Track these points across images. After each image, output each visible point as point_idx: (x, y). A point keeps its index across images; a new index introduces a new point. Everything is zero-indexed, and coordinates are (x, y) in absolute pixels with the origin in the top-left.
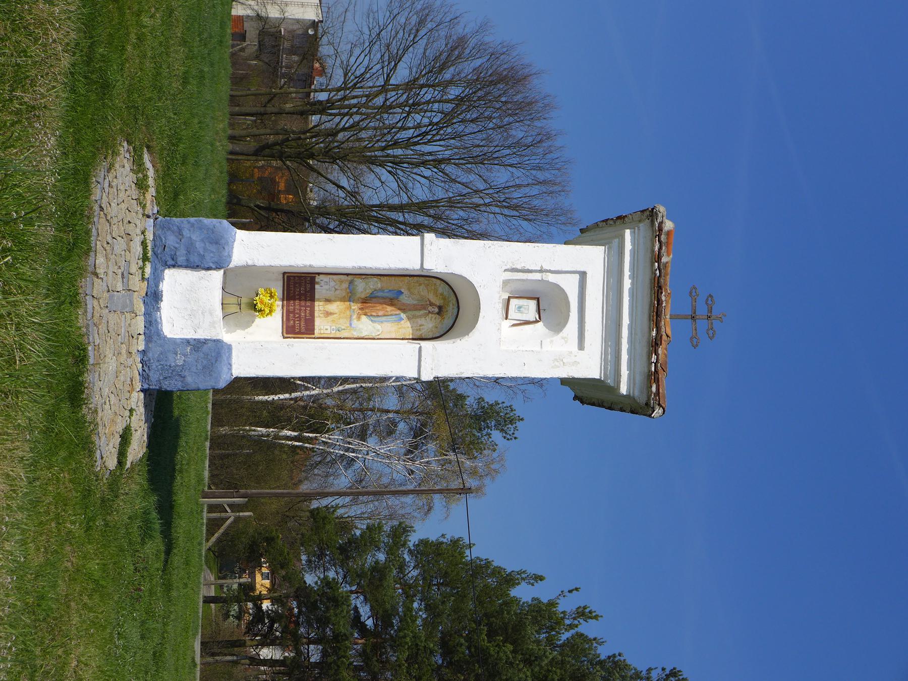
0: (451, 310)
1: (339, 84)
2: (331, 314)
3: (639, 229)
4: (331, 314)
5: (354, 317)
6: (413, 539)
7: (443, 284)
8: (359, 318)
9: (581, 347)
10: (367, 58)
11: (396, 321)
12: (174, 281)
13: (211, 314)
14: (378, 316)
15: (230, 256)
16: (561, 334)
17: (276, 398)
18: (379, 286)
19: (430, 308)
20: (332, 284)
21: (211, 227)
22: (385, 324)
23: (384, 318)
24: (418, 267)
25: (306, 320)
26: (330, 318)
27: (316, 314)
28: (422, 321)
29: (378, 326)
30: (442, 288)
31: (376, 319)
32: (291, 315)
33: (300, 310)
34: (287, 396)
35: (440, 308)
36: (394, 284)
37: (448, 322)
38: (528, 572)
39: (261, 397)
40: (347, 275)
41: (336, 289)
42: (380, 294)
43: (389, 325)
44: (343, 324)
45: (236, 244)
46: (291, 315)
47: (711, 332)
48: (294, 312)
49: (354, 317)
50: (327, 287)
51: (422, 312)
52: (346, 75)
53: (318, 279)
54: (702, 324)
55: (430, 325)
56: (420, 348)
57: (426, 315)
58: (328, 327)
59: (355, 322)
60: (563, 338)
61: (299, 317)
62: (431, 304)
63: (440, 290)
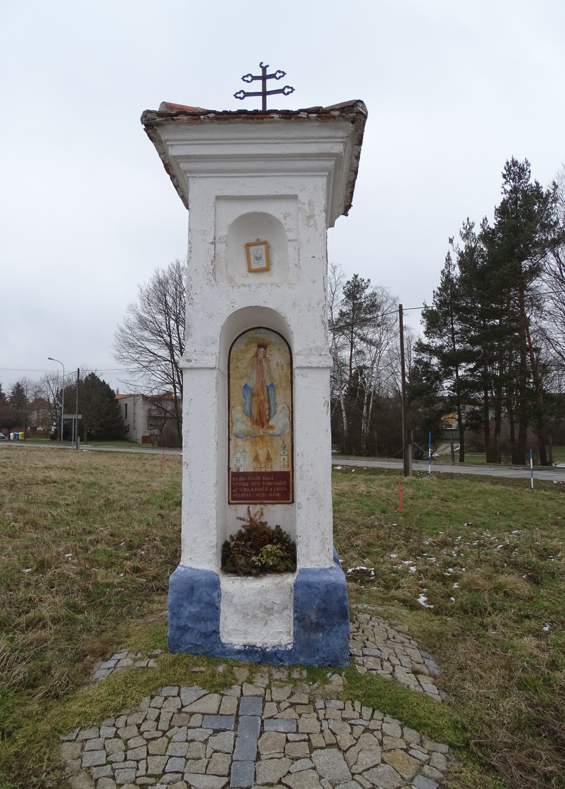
0: (261, 335)
1: (172, 387)
3: (168, 140)
5: (271, 432)
7: (236, 344)
8: (272, 427)
9: (294, 197)
10: (157, 372)
11: (274, 391)
12: (235, 632)
13: (267, 591)
14: (269, 408)
15: (207, 573)
16: (282, 221)
17: (345, 419)
18: (239, 408)
19: (261, 356)
20: (238, 455)
21: (176, 594)
22: (277, 401)
23: (272, 402)
24: (215, 373)
26: (273, 456)
27: (269, 470)
28: (273, 364)
29: (280, 407)
30: (240, 345)
32: (271, 495)
33: (265, 486)
34: (344, 412)
35: (260, 346)
36: (237, 394)
37: (273, 338)
40: (229, 440)
41: (244, 451)
42: (247, 407)
43: (278, 396)
44: (278, 443)
45: (194, 566)
46: (271, 495)
48: (268, 493)
49: (271, 432)
50: (242, 460)
51: (264, 365)
52: (167, 383)
53: (234, 470)
55: (278, 355)
56: (298, 368)
57: (268, 361)
58: (282, 458)
59: (276, 431)
60: (285, 218)
61: (272, 487)
62: (256, 355)
63: (243, 347)
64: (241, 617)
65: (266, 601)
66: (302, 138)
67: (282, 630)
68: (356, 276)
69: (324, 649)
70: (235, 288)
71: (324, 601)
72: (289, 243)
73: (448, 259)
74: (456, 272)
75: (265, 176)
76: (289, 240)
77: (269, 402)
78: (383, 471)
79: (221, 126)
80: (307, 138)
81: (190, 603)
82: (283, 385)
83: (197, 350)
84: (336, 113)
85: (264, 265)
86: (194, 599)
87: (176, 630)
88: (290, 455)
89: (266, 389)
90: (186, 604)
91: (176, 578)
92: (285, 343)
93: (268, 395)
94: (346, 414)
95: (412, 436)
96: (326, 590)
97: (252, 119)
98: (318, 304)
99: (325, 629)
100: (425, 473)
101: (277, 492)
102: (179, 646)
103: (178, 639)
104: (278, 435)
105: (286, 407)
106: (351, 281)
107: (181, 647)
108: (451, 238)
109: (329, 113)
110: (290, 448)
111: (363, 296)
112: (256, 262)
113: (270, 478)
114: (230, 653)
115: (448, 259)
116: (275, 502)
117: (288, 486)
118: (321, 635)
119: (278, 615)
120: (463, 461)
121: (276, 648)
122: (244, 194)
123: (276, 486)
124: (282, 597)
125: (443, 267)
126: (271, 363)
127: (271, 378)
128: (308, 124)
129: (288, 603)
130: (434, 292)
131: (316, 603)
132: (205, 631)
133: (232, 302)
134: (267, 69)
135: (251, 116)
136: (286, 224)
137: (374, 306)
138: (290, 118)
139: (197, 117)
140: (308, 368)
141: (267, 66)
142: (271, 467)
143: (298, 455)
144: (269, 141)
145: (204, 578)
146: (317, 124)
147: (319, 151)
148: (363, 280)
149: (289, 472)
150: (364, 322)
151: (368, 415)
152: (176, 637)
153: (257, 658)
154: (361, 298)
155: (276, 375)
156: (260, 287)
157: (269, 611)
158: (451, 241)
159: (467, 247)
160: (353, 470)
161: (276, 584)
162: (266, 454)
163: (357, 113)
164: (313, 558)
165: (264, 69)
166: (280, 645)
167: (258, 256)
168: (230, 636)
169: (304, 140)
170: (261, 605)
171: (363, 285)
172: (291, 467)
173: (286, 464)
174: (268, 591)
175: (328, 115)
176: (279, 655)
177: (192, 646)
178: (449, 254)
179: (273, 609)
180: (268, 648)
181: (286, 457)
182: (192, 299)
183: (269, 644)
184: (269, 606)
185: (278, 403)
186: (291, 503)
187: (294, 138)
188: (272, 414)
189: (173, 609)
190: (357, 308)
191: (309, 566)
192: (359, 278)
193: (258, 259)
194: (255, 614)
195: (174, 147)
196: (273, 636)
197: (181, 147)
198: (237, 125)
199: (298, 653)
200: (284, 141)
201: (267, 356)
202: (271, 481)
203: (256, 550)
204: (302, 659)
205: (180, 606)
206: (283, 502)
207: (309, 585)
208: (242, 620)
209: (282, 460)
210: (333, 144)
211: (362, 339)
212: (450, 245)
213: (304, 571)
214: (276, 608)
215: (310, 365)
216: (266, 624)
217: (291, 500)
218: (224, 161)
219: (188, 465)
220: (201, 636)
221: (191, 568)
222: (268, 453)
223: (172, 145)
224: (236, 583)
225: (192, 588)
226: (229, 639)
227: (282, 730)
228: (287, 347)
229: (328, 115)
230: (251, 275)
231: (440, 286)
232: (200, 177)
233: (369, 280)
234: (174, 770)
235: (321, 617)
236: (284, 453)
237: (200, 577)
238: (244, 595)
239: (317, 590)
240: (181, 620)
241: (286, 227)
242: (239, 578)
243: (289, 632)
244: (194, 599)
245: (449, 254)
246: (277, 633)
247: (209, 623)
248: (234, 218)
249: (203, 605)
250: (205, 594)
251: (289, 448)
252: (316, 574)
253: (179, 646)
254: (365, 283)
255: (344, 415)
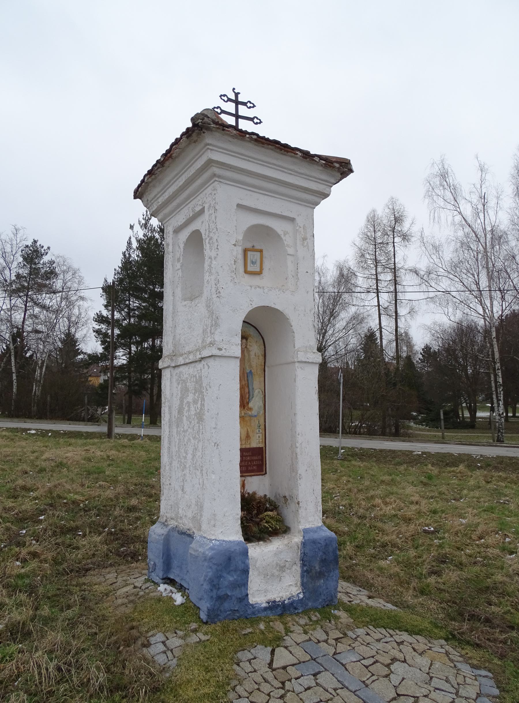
2: (248, 433)
4: (248, 433)
6: (105, 313)
8: (251, 409)
9: (292, 220)
11: (252, 377)
14: (249, 392)
16: (282, 236)
17: (15, 381)
23: (250, 387)
25: (253, 455)
26: (251, 434)
27: (248, 446)
28: (252, 354)
29: (256, 392)
31: (251, 394)
32: (249, 468)
34: (14, 375)
38: (124, 251)
39: (14, 390)
43: (255, 382)
45: (226, 539)
47: (256, 120)
49: (250, 413)
51: (246, 354)
54: (243, 111)
55: (256, 347)
57: (248, 351)
59: (254, 412)
60: (285, 235)
61: (250, 461)
64: (262, 578)
65: (281, 561)
66: (308, 176)
67: (291, 583)
68: (35, 242)
69: (325, 592)
70: (253, 288)
71: (324, 553)
72: (288, 256)
73: (129, 243)
74: (135, 255)
75: (273, 197)
76: (288, 255)
77: (248, 387)
78: (82, 435)
79: (256, 147)
80: (311, 177)
81: (228, 573)
82: (258, 373)
83: (224, 340)
84: (337, 165)
85: (258, 270)
86: (232, 568)
87: (216, 601)
88: (264, 433)
89: (246, 375)
90: (225, 575)
91: (214, 551)
92: (260, 337)
93: (248, 380)
94: (17, 376)
95: (86, 400)
96: (325, 544)
97: (281, 150)
98: (310, 311)
99: (325, 576)
100: (139, 437)
101: (254, 465)
102: (219, 615)
103: (218, 609)
104: (255, 416)
105: (261, 392)
106: (29, 245)
107: (220, 616)
108: (132, 224)
109: (332, 163)
110: (263, 427)
111: (41, 262)
112: (252, 265)
113: (249, 454)
114: (259, 612)
115: (129, 243)
116: (253, 474)
117: (262, 460)
118: (322, 581)
119: (289, 571)
120: (130, 423)
121: (291, 600)
122: (258, 208)
123: (253, 461)
124: (291, 555)
125: (124, 249)
126: (251, 353)
127: (250, 366)
128: (316, 167)
129: (296, 559)
130: (115, 270)
131: (319, 555)
132: (240, 596)
133: (250, 301)
134: (239, 95)
135: (283, 148)
136: (285, 240)
137: (52, 274)
138: (306, 158)
139: (243, 134)
140: (305, 362)
141: (239, 93)
142: (250, 444)
143: (299, 435)
144: (286, 170)
145: (237, 548)
146: (321, 168)
147: (317, 189)
148: (43, 247)
149: (262, 448)
150: (40, 288)
151: (41, 378)
152: (216, 607)
153: (279, 611)
154: (39, 263)
155: (254, 364)
156: (271, 290)
157: (282, 568)
158: (132, 227)
159: (145, 235)
160: (50, 434)
161: (286, 545)
162: (246, 433)
163: (349, 169)
164: (310, 519)
165: (237, 94)
166: (293, 596)
167: (254, 261)
168: (254, 597)
169: (308, 177)
170: (277, 565)
171: (43, 251)
172: (264, 444)
173: (261, 441)
174: (281, 552)
175: (332, 165)
176: (295, 605)
177: (230, 612)
178: (130, 238)
179: (285, 566)
180: (285, 600)
181: (260, 435)
182: (219, 292)
183: (284, 597)
184: (282, 565)
185: (255, 388)
186: (264, 474)
187: (302, 174)
188: (251, 397)
189: (213, 581)
190: (34, 272)
191: (308, 526)
192: (38, 244)
193: (253, 263)
194: (273, 574)
195: (213, 151)
196: (286, 590)
197: (219, 153)
198: (268, 151)
199: (308, 599)
200: (296, 174)
201: (248, 347)
202: (249, 456)
203: (260, 518)
204: (310, 604)
205: (220, 577)
206: (258, 473)
207: (314, 542)
208: (263, 581)
209: (257, 438)
210: (326, 187)
211: (35, 303)
212: (131, 230)
213: (306, 531)
214: (287, 565)
215: (307, 360)
216: (280, 581)
217: (264, 472)
218: (248, 176)
219: (218, 445)
220: (237, 601)
221: (224, 541)
222: (248, 431)
223: (211, 150)
224: (256, 548)
225: (229, 559)
226: (254, 600)
227: (355, 660)
228: (262, 341)
229: (332, 165)
230: (246, 276)
231: (120, 265)
232: (225, 183)
233: (49, 248)
234: (406, 697)
235: (323, 567)
236: (259, 431)
237: (235, 548)
238: (264, 558)
239: (319, 545)
240: (220, 590)
241: (286, 243)
242: (253, 544)
243: (296, 584)
244: (232, 568)
245: (130, 238)
246: (287, 587)
247: (243, 587)
248: (248, 226)
249: (238, 573)
250: (240, 562)
251: (262, 427)
252: (316, 532)
253: (219, 615)
254: (45, 250)
255: (14, 377)
